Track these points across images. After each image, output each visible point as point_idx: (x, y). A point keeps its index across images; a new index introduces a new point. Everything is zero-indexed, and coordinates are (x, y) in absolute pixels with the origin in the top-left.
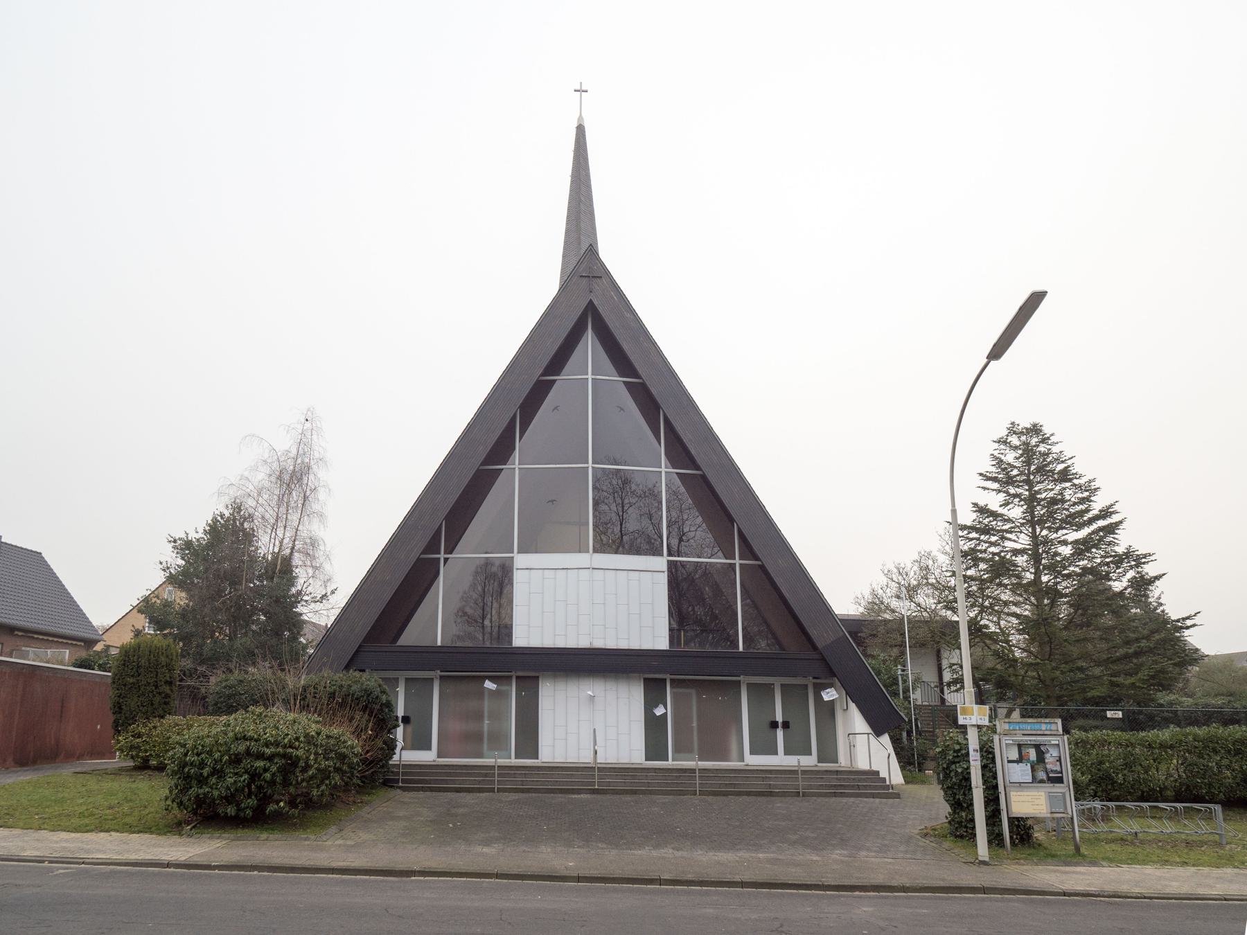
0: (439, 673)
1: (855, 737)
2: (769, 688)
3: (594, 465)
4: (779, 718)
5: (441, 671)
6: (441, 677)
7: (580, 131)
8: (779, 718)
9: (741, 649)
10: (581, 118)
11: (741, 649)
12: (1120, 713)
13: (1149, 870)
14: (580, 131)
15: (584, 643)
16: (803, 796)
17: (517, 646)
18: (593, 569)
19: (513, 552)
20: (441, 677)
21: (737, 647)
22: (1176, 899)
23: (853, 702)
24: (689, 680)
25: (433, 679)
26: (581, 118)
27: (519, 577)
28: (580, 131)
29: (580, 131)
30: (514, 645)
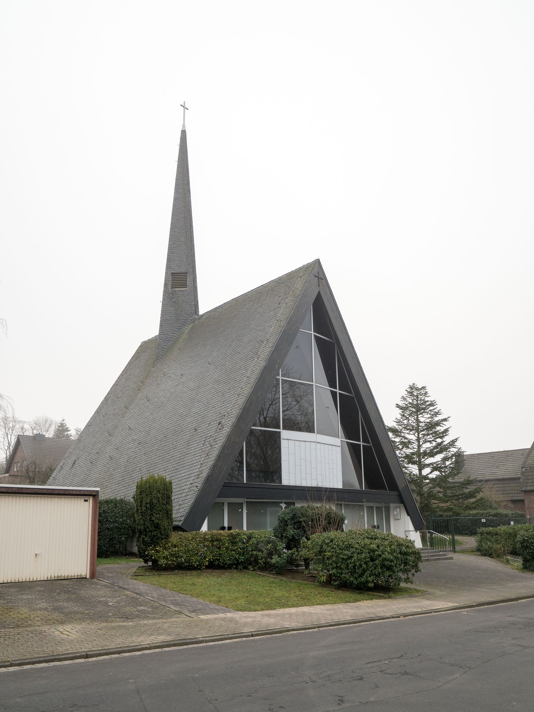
0: (246, 500)
1: (410, 533)
2: (372, 508)
3: (316, 384)
4: (226, 525)
5: (247, 499)
6: (247, 502)
7: (184, 133)
8: (226, 525)
9: (245, 482)
10: (184, 125)
11: (245, 482)
12: (485, 520)
13: (147, 652)
14: (184, 133)
15: (314, 485)
16: (430, 561)
17: (284, 485)
18: (317, 442)
19: (341, 438)
20: (247, 502)
21: (363, 489)
22: (445, 611)
23: (408, 515)
24: (259, 502)
25: (243, 503)
26: (184, 125)
27: (284, 444)
28: (184, 133)
29: (184, 133)
30: (283, 484)
